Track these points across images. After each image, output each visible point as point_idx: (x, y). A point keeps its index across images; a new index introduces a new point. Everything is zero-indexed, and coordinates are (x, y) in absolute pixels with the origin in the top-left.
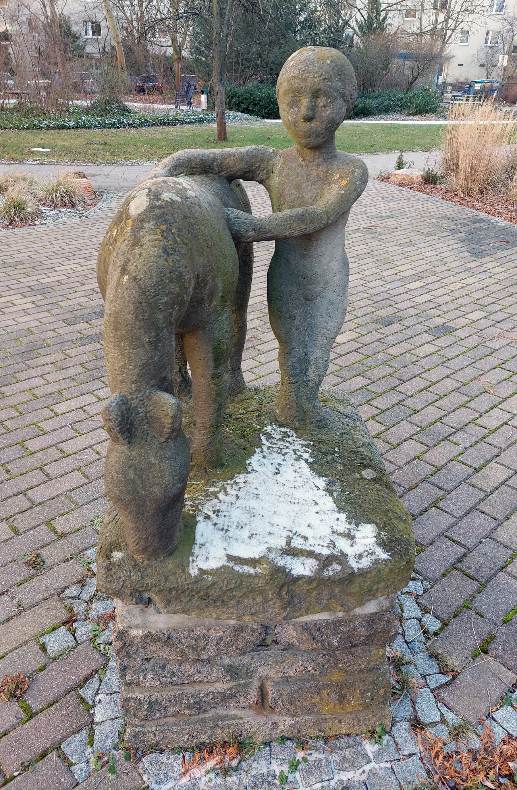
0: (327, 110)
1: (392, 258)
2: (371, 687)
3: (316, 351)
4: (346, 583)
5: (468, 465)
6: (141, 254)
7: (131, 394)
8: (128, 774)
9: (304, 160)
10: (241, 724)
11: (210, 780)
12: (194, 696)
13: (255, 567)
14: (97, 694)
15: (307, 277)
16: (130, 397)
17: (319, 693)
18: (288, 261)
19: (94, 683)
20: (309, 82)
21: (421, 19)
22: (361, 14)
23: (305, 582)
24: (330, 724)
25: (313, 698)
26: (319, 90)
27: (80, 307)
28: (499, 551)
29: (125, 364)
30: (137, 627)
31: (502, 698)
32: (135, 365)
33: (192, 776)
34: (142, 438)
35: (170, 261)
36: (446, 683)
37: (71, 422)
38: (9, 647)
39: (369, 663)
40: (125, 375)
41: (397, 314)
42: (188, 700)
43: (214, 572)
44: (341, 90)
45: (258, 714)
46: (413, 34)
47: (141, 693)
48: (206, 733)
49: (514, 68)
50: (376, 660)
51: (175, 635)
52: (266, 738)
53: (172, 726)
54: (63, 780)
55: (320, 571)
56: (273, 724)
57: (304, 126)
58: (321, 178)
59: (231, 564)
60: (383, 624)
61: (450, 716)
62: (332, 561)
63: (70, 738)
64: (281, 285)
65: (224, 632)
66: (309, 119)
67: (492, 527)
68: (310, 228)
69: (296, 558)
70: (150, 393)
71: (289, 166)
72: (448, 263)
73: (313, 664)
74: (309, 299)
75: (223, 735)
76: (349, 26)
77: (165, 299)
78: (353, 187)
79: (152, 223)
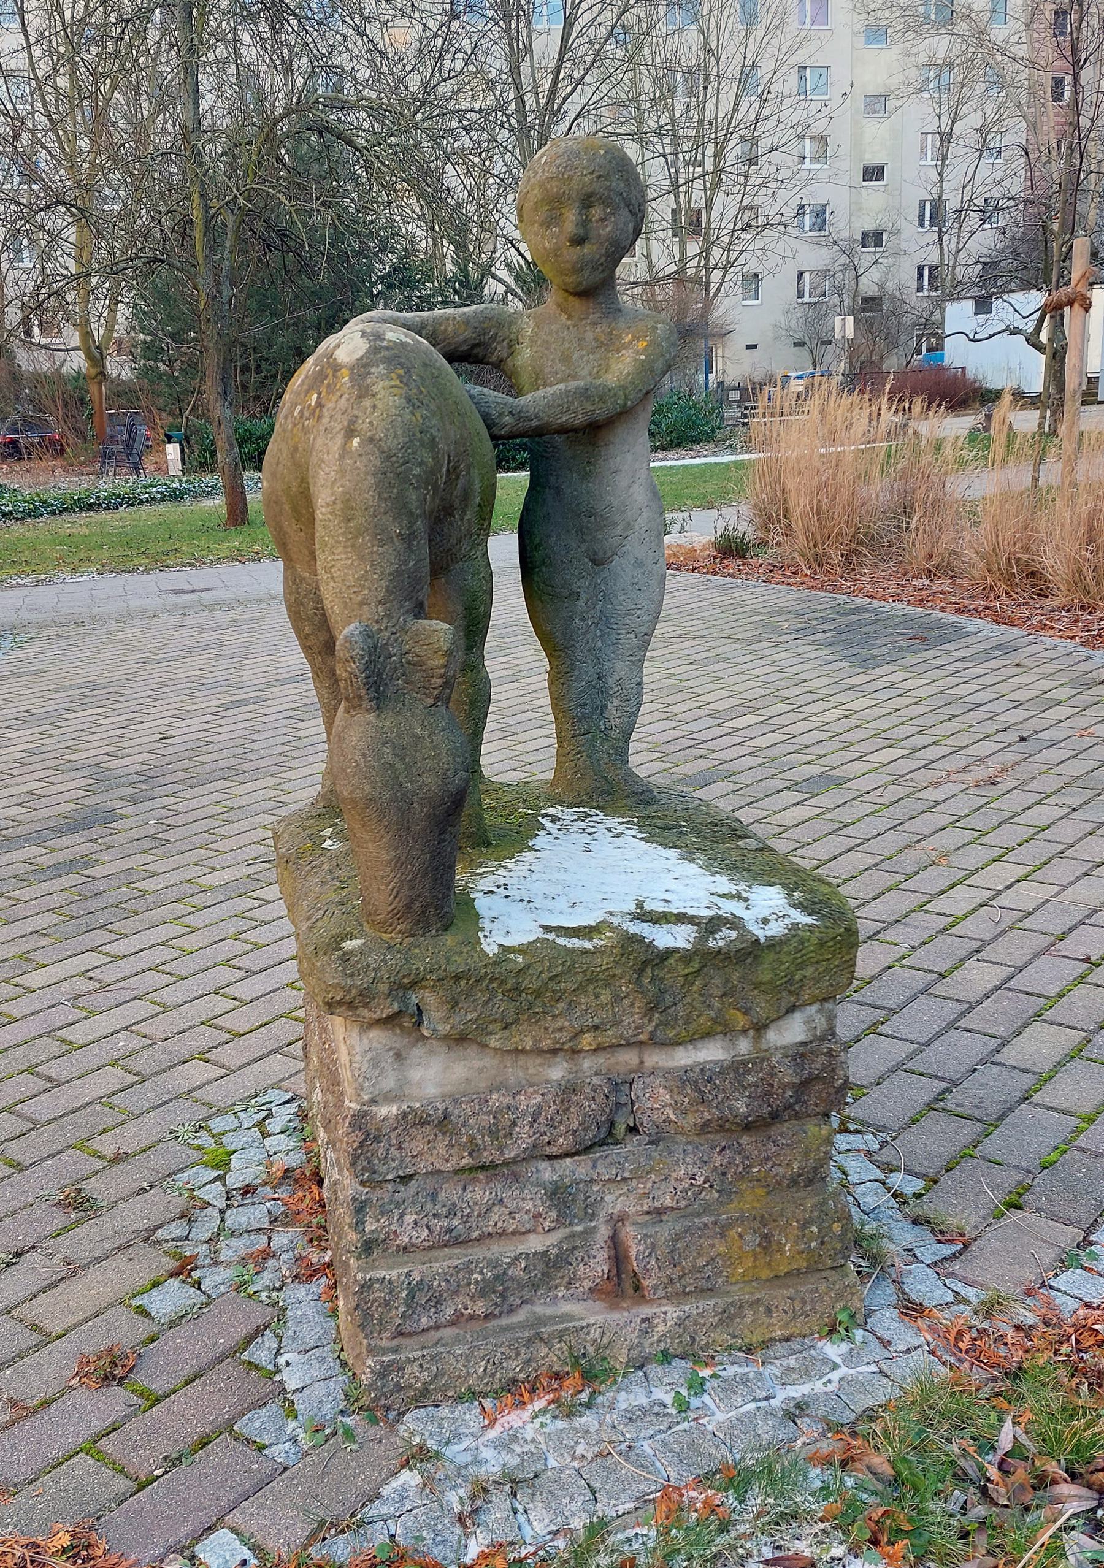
0: (607, 226)
1: (683, 684)
2: (815, 1214)
3: (619, 665)
4: (749, 961)
5: (924, 970)
6: (374, 407)
7: (377, 622)
8: (380, 1442)
9: (569, 317)
10: (583, 1328)
11: (542, 1425)
12: (494, 1264)
13: (591, 940)
14: (278, 1353)
15: (595, 514)
16: (376, 627)
17: (722, 1235)
18: (558, 491)
19: (269, 1340)
20: (575, 184)
21: (648, 257)
22: (517, 250)
23: (680, 958)
24: (749, 1321)
25: (713, 1246)
26: (590, 195)
27: (11, 824)
28: (1013, 1078)
29: (366, 572)
30: (389, 1098)
31: (1062, 1261)
32: (382, 573)
33: (506, 1425)
34: (397, 701)
35: (418, 415)
36: (954, 1254)
37: (68, 997)
38: (71, 1321)
39: (806, 1154)
40: (366, 592)
41: (720, 767)
42: (481, 1273)
43: (522, 950)
44: (624, 194)
45: (614, 1307)
46: (637, 284)
47: (391, 1268)
48: (518, 1354)
49: (871, 342)
50: (818, 1149)
51: (456, 1112)
52: (634, 1353)
53: (453, 1344)
54: (255, 1467)
55: (702, 939)
56: (644, 1320)
57: (573, 254)
58: (602, 342)
59: (551, 936)
60: (821, 1060)
61: (970, 1293)
62: (719, 926)
63: (249, 1415)
64: (549, 536)
65: (542, 1095)
66: (578, 241)
67: (990, 1048)
68: (601, 412)
69: (657, 926)
70: (405, 621)
71: (546, 329)
72: (805, 681)
73: (706, 1171)
74: (598, 561)
75: (551, 1357)
76: (494, 277)
77: (417, 471)
78: (658, 351)
79: (381, 366)
